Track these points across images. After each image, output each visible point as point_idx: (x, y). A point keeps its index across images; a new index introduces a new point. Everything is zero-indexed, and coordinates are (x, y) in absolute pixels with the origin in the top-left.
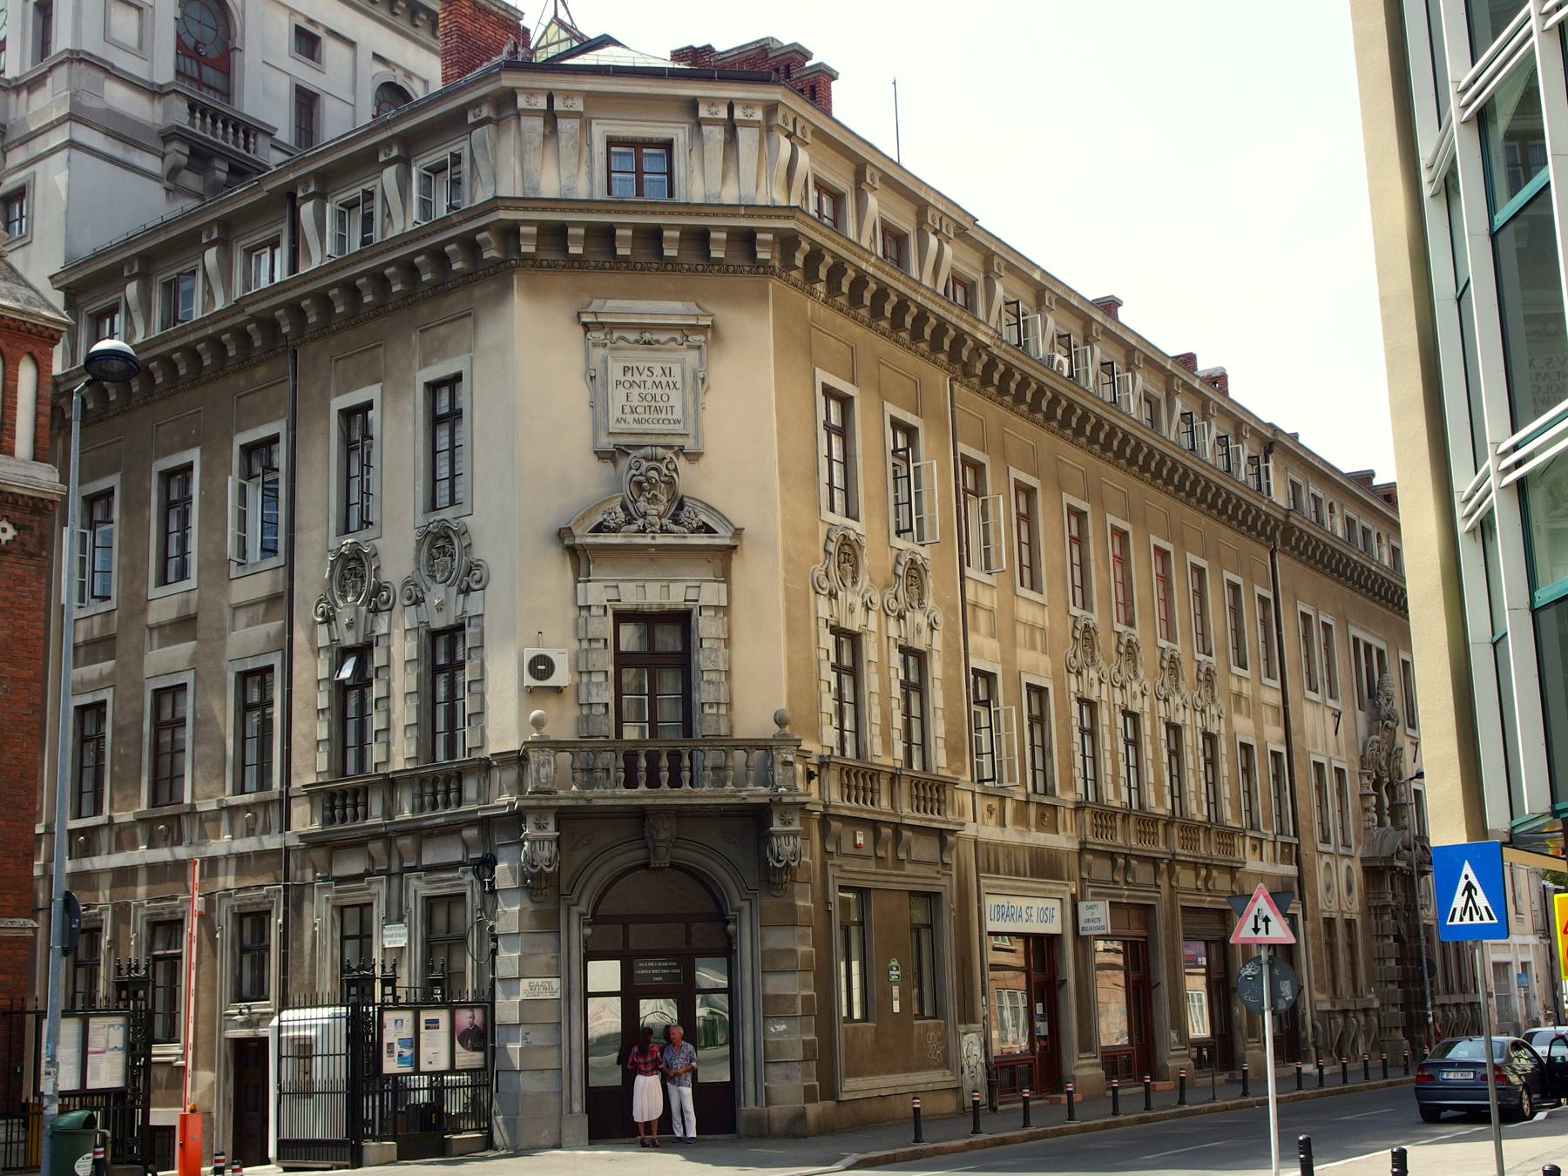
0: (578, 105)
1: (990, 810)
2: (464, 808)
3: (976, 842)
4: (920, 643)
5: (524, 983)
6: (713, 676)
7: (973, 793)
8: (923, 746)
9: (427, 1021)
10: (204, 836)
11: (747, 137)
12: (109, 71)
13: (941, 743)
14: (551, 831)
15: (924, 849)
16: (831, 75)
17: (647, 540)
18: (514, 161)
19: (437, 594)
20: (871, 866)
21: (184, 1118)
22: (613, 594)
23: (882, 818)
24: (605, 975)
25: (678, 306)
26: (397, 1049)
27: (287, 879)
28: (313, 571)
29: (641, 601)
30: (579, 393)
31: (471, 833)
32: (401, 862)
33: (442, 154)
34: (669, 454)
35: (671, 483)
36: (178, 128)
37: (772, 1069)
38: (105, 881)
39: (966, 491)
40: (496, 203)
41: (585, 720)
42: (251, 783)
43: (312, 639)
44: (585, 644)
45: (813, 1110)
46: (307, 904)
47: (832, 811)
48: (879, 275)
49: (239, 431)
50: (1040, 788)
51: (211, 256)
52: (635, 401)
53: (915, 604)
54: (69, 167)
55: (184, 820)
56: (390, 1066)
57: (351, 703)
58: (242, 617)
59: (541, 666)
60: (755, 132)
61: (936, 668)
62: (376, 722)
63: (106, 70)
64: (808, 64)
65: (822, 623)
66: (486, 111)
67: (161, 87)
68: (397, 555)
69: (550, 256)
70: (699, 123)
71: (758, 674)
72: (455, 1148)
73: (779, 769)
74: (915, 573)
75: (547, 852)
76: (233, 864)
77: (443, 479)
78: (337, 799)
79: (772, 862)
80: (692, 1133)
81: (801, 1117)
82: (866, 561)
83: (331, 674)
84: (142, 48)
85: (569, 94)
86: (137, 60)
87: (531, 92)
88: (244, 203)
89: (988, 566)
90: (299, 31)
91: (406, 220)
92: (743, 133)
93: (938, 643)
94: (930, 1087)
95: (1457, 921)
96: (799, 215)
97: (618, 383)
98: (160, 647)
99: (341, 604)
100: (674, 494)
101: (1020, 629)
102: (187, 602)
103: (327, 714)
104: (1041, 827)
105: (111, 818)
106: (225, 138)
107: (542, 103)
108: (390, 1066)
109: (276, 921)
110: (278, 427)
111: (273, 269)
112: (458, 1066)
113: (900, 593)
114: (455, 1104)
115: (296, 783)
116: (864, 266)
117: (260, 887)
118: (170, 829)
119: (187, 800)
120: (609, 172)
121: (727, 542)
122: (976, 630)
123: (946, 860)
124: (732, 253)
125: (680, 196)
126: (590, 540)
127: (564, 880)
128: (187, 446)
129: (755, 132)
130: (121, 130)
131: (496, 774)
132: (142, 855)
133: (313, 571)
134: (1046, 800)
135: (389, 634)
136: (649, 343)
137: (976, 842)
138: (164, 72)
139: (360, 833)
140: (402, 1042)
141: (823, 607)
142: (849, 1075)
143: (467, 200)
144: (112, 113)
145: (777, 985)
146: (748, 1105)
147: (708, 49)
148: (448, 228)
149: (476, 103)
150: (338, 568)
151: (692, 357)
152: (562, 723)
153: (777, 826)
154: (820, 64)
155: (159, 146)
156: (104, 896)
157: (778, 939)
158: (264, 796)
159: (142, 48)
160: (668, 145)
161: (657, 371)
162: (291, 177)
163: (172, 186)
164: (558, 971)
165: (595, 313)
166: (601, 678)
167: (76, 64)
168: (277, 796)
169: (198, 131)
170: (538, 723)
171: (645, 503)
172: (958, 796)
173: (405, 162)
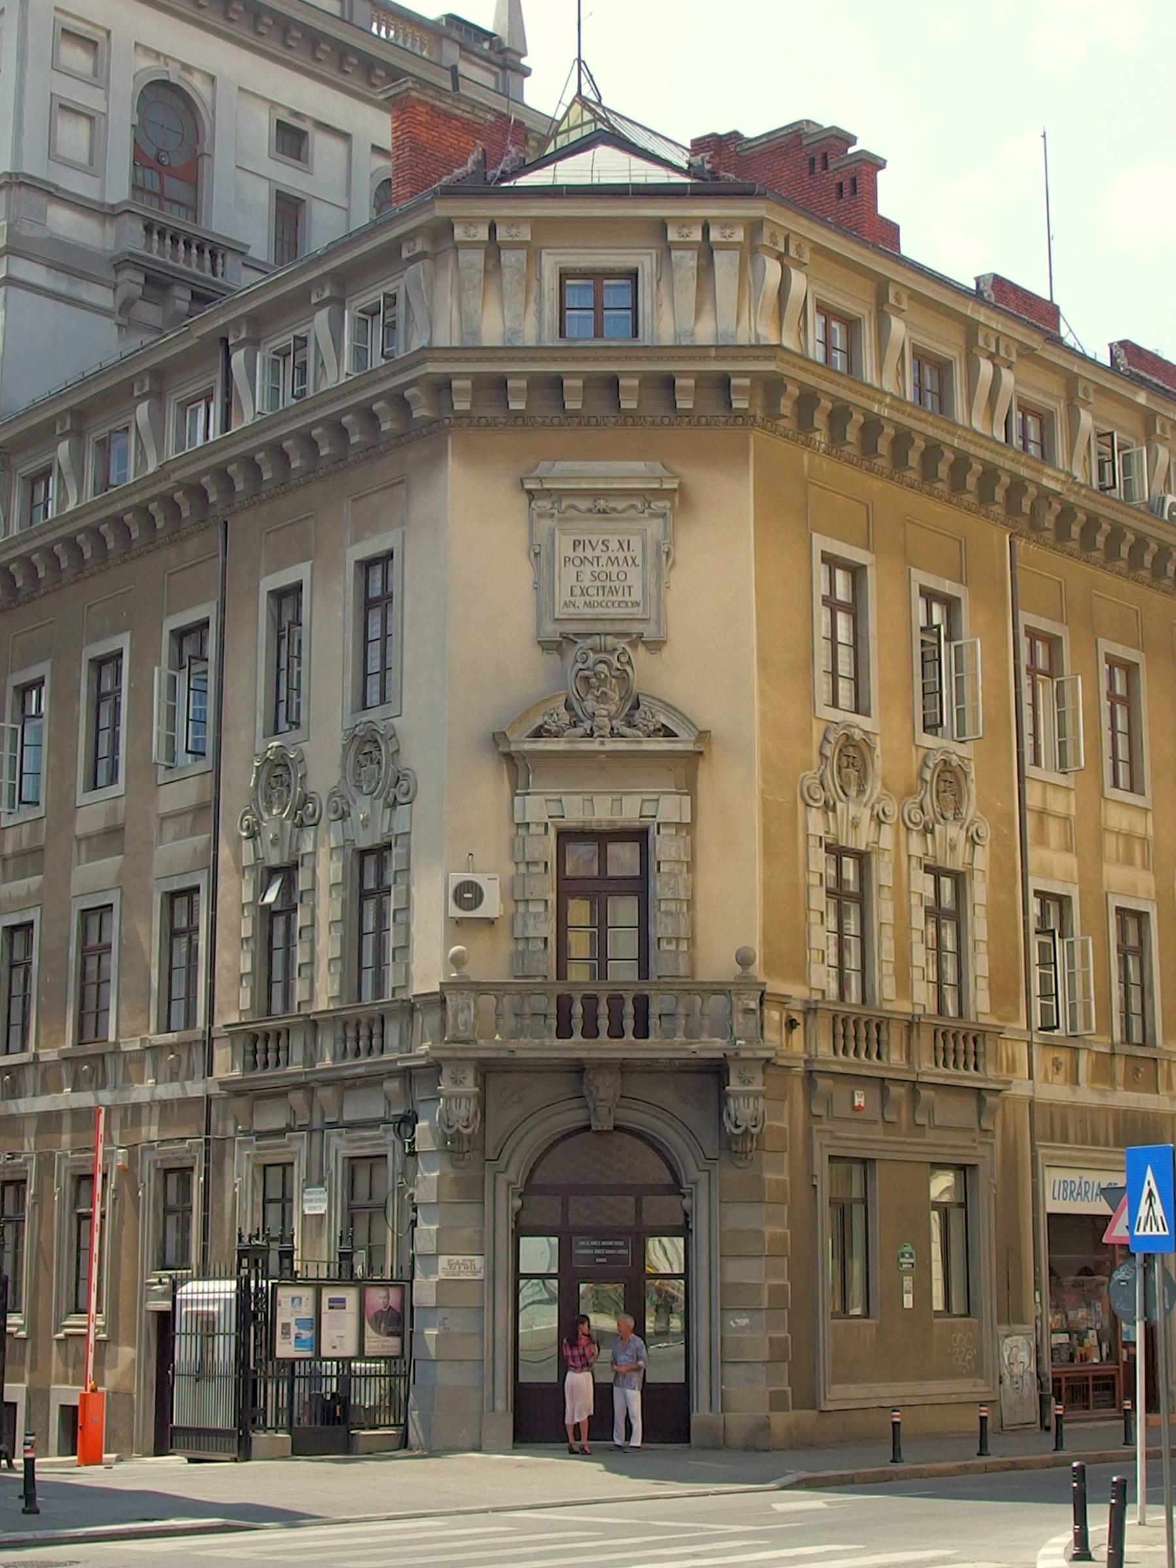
0: (525, 234)
1: (1056, 1064)
2: (385, 1057)
3: (1032, 1103)
4: (956, 862)
5: (443, 1260)
6: (672, 906)
7: (1030, 1044)
8: (959, 987)
9: (331, 1301)
10: (128, 1080)
11: (725, 263)
12: (53, 194)
13: (983, 983)
14: (469, 1086)
15: (959, 1112)
16: (874, 164)
17: (596, 746)
18: (450, 301)
19: (362, 808)
20: (878, 1132)
21: (84, 1397)
22: (555, 810)
23: (891, 1075)
24: (539, 1253)
25: (639, 466)
26: (294, 1330)
27: (208, 1132)
28: (241, 778)
29: (588, 817)
30: (521, 571)
31: (392, 1086)
32: (323, 1117)
33: (374, 295)
34: (622, 644)
35: (623, 677)
36: (131, 254)
37: (730, 1369)
38: (31, 1126)
39: (1033, 670)
40: (429, 352)
41: (520, 957)
42: (177, 1019)
43: (237, 857)
44: (522, 868)
45: (781, 1420)
46: (227, 1161)
47: (817, 1067)
48: (897, 417)
49: (170, 613)
50: (1136, 1036)
51: (142, 411)
52: (587, 581)
53: (949, 815)
54: (5, 307)
55: (108, 1058)
56: (285, 1349)
57: (276, 927)
58: (170, 829)
59: (468, 895)
60: (735, 256)
61: (979, 892)
62: (300, 956)
63: (49, 193)
64: (851, 150)
65: (813, 841)
66: (420, 245)
67: (113, 206)
68: (323, 763)
69: (489, 412)
70: (669, 248)
71: (731, 900)
72: (361, 1445)
73: (739, 1018)
74: (950, 778)
75: (464, 1111)
76: (156, 1112)
77: (374, 678)
78: (261, 1044)
79: (729, 1127)
80: (636, 1441)
81: (765, 1427)
82: (878, 764)
83: (255, 899)
84: (94, 165)
85: (514, 222)
86: (89, 178)
87: (470, 222)
88: (174, 351)
89: (1063, 763)
90: (280, 125)
91: (335, 370)
92: (719, 258)
93: (982, 858)
94: (954, 1398)
95: (1141, 1232)
96: (781, 354)
97: (567, 560)
98: (87, 861)
99: (266, 817)
100: (628, 690)
101: (1110, 841)
102: (114, 810)
103: (251, 943)
104: (1132, 1083)
105: (36, 1056)
106: (187, 262)
107: (483, 234)
108: (285, 1349)
109: (198, 1179)
110: (206, 610)
111: (205, 427)
112: (369, 1351)
113: (927, 801)
114: (368, 1396)
115: (218, 1023)
116: (876, 409)
117: (183, 1139)
118: (94, 1070)
119: (112, 1038)
120: (562, 309)
121: (691, 747)
122: (1043, 841)
123: (985, 1125)
124: (710, 402)
125: (646, 337)
126: (527, 747)
127: (491, 1142)
128: (116, 631)
129: (735, 256)
130: (67, 260)
131: (419, 1017)
132: (66, 1099)
133: (241, 778)
134: (1140, 1052)
135: (314, 853)
136: (605, 512)
137: (1032, 1103)
138: (117, 186)
139: (280, 1082)
140: (300, 1323)
141: (816, 823)
142: (838, 1379)
143: (401, 348)
144: (56, 242)
145: (741, 1272)
146: (701, 1413)
147: (735, 136)
148: (375, 382)
149: (409, 236)
150: (264, 775)
151: (655, 528)
152: (490, 962)
153: (734, 1085)
154: (861, 152)
155: (110, 276)
156: (29, 1144)
157: (740, 1217)
158: (189, 1035)
159: (94, 165)
160: (633, 275)
161: (614, 545)
162: (221, 321)
163: (125, 322)
164: (482, 1248)
165: (540, 479)
166: (540, 908)
167: (15, 189)
168: (200, 1037)
169: (155, 257)
170: (457, 961)
171: (597, 698)
172: (1005, 1049)
173: (338, 302)
